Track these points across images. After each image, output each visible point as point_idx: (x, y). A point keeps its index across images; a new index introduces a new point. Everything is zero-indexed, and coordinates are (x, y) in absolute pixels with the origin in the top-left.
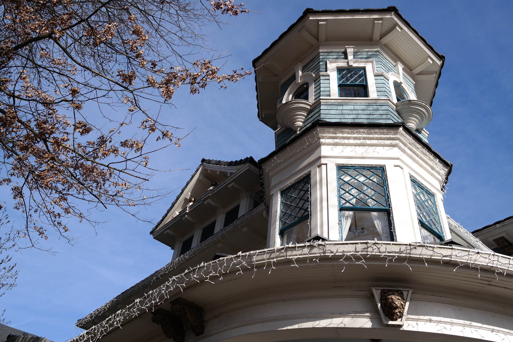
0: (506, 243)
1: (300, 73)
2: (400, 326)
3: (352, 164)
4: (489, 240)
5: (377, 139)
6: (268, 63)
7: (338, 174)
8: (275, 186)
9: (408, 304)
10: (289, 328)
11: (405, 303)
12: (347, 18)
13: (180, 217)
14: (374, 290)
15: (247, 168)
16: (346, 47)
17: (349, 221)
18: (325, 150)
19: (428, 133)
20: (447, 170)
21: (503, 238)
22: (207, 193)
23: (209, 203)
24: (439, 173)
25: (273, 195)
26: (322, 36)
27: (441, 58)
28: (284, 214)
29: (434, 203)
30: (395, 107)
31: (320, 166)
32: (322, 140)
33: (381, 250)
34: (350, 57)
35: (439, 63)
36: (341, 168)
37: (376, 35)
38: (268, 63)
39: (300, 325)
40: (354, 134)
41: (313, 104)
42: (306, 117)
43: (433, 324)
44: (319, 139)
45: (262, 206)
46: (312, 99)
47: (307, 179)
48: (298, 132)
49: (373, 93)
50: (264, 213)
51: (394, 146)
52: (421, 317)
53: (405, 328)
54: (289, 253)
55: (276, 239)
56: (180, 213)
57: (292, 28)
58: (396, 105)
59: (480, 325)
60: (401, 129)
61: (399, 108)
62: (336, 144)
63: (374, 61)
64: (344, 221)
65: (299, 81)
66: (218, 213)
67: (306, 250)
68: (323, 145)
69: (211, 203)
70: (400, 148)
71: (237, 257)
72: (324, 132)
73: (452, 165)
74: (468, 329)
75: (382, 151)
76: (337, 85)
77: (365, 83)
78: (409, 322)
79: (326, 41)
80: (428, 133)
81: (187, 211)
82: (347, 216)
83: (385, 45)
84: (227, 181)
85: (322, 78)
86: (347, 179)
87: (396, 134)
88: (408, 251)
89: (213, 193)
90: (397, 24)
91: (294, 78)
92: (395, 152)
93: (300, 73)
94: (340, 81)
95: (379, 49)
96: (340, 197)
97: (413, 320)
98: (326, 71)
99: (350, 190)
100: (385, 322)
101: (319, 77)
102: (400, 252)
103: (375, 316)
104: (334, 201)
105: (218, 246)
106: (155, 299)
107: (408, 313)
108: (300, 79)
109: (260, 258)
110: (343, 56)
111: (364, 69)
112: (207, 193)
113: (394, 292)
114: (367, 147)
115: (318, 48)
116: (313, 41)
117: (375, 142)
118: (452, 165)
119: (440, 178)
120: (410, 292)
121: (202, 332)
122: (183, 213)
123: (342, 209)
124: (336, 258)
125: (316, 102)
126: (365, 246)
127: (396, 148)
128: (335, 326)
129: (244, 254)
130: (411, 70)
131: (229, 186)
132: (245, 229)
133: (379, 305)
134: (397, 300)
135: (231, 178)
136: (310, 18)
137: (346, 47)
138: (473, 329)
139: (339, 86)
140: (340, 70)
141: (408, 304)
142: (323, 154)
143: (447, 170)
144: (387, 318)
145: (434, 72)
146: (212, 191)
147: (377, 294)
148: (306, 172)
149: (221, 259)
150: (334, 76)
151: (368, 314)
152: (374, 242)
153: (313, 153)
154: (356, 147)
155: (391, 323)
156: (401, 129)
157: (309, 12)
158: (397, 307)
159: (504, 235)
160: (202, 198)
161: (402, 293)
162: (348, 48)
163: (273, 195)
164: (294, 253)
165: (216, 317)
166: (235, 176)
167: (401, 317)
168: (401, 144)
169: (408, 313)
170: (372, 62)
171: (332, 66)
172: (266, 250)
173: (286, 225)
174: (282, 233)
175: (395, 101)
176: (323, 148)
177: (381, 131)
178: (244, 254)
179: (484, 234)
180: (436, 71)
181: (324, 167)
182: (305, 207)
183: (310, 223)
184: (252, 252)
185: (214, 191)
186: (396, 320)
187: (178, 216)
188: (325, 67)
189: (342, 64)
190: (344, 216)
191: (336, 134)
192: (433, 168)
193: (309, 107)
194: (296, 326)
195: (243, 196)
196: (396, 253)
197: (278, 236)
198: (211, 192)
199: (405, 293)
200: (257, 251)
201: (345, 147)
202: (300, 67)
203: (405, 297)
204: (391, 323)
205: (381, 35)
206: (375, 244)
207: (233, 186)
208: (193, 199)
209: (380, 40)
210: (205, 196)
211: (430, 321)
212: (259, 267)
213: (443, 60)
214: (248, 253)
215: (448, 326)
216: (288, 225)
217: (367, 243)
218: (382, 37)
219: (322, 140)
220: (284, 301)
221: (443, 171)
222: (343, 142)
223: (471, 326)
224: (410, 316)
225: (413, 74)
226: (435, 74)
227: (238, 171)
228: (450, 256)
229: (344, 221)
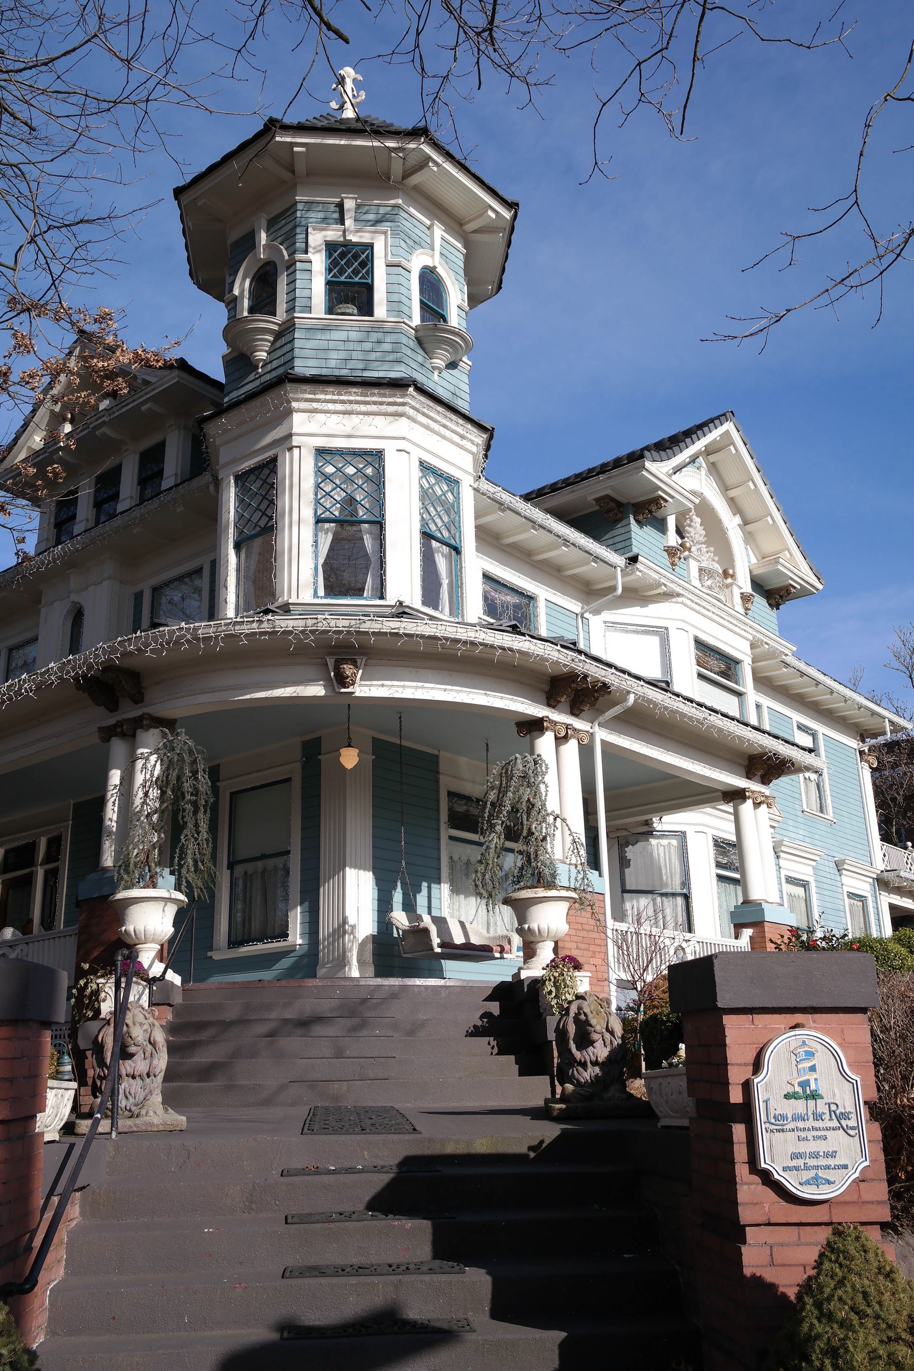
0: (612, 505)
1: (263, 235)
2: (353, 693)
3: (336, 448)
4: (588, 499)
5: (375, 403)
6: (203, 201)
7: (316, 460)
8: (227, 464)
9: (361, 671)
10: (240, 698)
11: (358, 671)
12: (343, 142)
13: (47, 454)
14: (328, 659)
15: (176, 380)
16: (343, 195)
17: (330, 537)
18: (300, 422)
19: (470, 363)
20: (485, 436)
21: (608, 497)
22: (100, 415)
23: (104, 434)
24: (472, 442)
25: (222, 479)
26: (301, 167)
27: (512, 205)
28: (240, 517)
29: (457, 498)
30: (413, 331)
31: (290, 449)
32: (295, 405)
33: (331, 625)
34: (349, 222)
35: (507, 215)
36: (321, 453)
37: (397, 169)
38: (203, 201)
39: (252, 695)
40: (342, 395)
41: (284, 323)
42: (273, 343)
43: (385, 689)
44: (289, 402)
45: (206, 477)
46: (281, 314)
47: (272, 464)
48: (260, 370)
49: (380, 310)
50: (212, 488)
51: (401, 415)
52: (375, 683)
53: (357, 694)
54: (237, 627)
55: (229, 557)
56: (47, 446)
57: (244, 146)
58: (416, 330)
59: (432, 685)
60: (411, 389)
61: (420, 334)
62: (315, 411)
63: (389, 232)
64: (322, 536)
65: (262, 257)
66: (125, 451)
67: (255, 625)
68: (296, 412)
69: (108, 433)
70: (409, 418)
71: (180, 628)
72: (296, 392)
73: (493, 429)
74: (420, 691)
75: (380, 425)
76: (323, 283)
77: (370, 281)
78: (362, 688)
79: (308, 175)
80: (470, 363)
81: (62, 444)
82: (328, 529)
83: (417, 189)
84: (139, 398)
85: (298, 264)
86: (330, 469)
87: (403, 396)
88: (358, 626)
89: (111, 417)
90: (430, 158)
91: (249, 241)
92: (402, 426)
93: (263, 235)
94: (329, 274)
95: (400, 201)
96: (317, 502)
97: (366, 685)
98: (306, 252)
99: (335, 489)
100: (337, 690)
101: (295, 263)
102: (350, 627)
103: (329, 684)
104: (308, 513)
105: (134, 531)
106: (80, 668)
107: (361, 679)
108: (264, 249)
109: (205, 631)
110: (336, 215)
111: (371, 246)
112: (100, 415)
113: (346, 661)
114: (361, 417)
115: (292, 189)
116: (286, 175)
117: (374, 408)
118: (493, 429)
119: (474, 449)
120: (364, 660)
121: (142, 701)
122: (52, 446)
123: (319, 521)
124: (287, 633)
125: (288, 321)
126: (315, 621)
127: (403, 418)
128: (289, 695)
129: (187, 626)
130: (461, 225)
131: (143, 408)
132: (180, 509)
133: (332, 674)
134: (348, 669)
135: (146, 394)
136: (278, 139)
137: (343, 195)
138: (425, 691)
139: (328, 283)
140: (330, 247)
141: (361, 671)
142: (295, 430)
143: (485, 436)
144: (339, 686)
145: (502, 228)
146: (111, 412)
147: (331, 662)
148: (270, 454)
149: (161, 629)
150: (318, 262)
151: (321, 683)
152: (324, 617)
153: (281, 424)
154: (345, 416)
155: (343, 690)
156: (411, 389)
157: (272, 126)
158: (348, 677)
159: (609, 492)
160: (91, 423)
161: (356, 662)
162: (346, 198)
163: (222, 479)
164: (243, 627)
165: (158, 683)
166: (154, 389)
167: (353, 684)
168: (411, 412)
169: (361, 679)
170: (385, 233)
171: (317, 238)
172: (212, 623)
173: (243, 536)
174: (238, 546)
175: (416, 321)
176: (297, 418)
177: (382, 391)
178: (187, 626)
179: (581, 489)
180: (504, 227)
181: (296, 451)
182: (269, 512)
183: (275, 542)
184: (196, 624)
185: (114, 412)
186: (348, 687)
187: (43, 451)
188: (304, 236)
189: (333, 234)
190: (322, 529)
191: (315, 394)
192: (462, 437)
193: (276, 328)
194: (248, 697)
195: (172, 425)
196: (345, 627)
197: (233, 550)
198: (106, 413)
199: (359, 661)
200: (203, 624)
201: (328, 415)
202: (264, 223)
203: (359, 665)
204: (343, 690)
205: (404, 172)
206: (325, 619)
207: (149, 409)
208: (69, 416)
209: (403, 180)
210: (97, 420)
211: (383, 685)
212: (207, 639)
213: (515, 209)
214: (192, 626)
215: (400, 690)
216: (245, 535)
217: (317, 618)
218: (407, 175)
219: (295, 405)
220: (236, 668)
221: (479, 438)
222: (326, 408)
223: (423, 687)
224: (363, 683)
225: (464, 231)
226: (502, 232)
227: (161, 382)
228: (398, 628)
229: (322, 536)
